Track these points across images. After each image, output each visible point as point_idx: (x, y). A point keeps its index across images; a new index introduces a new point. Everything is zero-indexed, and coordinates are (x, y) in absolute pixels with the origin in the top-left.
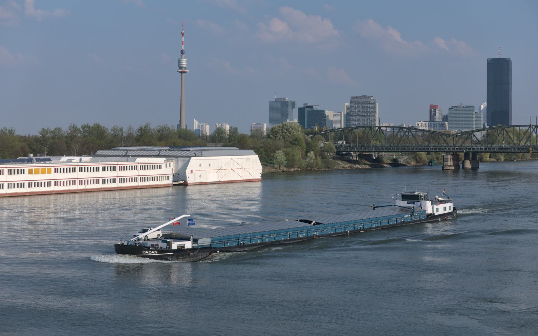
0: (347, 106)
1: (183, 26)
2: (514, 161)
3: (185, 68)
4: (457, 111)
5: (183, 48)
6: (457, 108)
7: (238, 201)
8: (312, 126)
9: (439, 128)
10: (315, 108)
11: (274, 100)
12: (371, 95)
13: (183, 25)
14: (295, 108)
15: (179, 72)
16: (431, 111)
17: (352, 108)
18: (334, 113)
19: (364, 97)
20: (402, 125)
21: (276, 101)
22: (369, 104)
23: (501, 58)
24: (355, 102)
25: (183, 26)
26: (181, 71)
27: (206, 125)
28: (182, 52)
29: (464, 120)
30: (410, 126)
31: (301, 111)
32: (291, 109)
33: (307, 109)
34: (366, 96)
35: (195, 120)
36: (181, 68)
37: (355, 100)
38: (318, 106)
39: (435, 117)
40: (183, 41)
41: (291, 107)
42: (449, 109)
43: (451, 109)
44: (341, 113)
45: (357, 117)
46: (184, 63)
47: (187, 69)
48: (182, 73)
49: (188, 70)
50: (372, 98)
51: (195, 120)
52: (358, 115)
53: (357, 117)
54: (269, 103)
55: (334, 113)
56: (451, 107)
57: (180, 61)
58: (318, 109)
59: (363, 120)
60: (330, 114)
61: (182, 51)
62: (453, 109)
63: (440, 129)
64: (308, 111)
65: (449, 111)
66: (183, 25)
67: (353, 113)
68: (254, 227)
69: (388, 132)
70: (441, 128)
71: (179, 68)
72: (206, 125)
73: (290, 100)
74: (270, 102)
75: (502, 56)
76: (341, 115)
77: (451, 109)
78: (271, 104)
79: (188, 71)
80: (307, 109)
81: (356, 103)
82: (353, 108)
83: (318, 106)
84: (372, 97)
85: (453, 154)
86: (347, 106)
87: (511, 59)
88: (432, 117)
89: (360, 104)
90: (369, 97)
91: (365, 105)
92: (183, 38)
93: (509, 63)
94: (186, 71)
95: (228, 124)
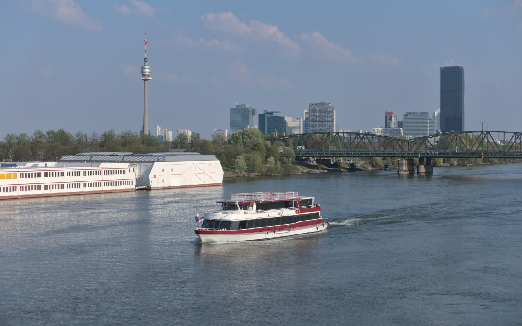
0: (306, 112)
2: (466, 166)
5: (146, 56)
6: (412, 115)
10: (275, 114)
11: (235, 107)
13: (146, 34)
14: (255, 114)
15: (142, 79)
16: (386, 117)
18: (293, 119)
19: (322, 104)
20: (359, 130)
21: (237, 108)
26: (144, 78)
27: (169, 131)
28: (145, 60)
31: (262, 117)
32: (251, 116)
36: (144, 75)
37: (314, 106)
39: (391, 123)
40: (146, 49)
41: (251, 113)
42: (404, 115)
43: (406, 115)
44: (300, 119)
46: (147, 71)
48: (144, 80)
49: (151, 77)
50: (330, 105)
51: (158, 127)
52: (316, 121)
55: (293, 119)
56: (11, 134)
57: (143, 68)
58: (278, 116)
60: (289, 121)
61: (145, 59)
62: (408, 115)
64: (268, 117)
65: (404, 117)
66: (146, 34)
74: (231, 108)
76: (300, 121)
77: (406, 115)
78: (232, 110)
79: (151, 78)
82: (312, 115)
83: (278, 112)
84: (330, 103)
85: (408, 159)
86: (306, 112)
87: (464, 67)
90: (327, 104)
91: (323, 112)
92: (146, 46)
93: (462, 71)
94: (149, 78)
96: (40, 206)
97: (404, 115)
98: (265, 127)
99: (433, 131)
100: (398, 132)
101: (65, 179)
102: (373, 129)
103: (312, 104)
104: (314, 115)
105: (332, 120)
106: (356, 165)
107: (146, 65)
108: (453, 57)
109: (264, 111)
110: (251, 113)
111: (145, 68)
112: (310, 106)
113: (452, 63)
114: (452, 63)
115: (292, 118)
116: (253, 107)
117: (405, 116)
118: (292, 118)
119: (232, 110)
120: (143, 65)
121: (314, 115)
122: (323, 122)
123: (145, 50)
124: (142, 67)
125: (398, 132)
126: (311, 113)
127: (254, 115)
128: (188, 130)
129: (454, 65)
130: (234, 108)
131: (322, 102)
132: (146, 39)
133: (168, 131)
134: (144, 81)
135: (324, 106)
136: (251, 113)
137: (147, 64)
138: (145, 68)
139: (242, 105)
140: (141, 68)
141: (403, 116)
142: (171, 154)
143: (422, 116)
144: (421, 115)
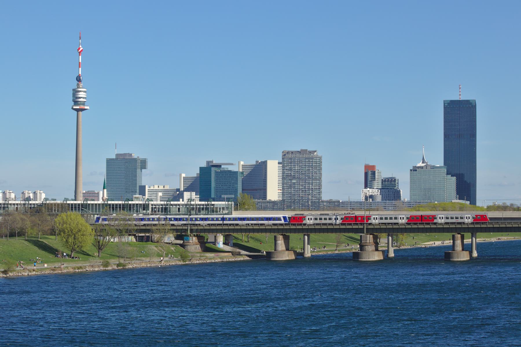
1: (80, 39)
3: (84, 103)
4: (427, 174)
6: (422, 170)
8: (223, 194)
9: (392, 199)
12: (314, 150)
13: (80, 37)
14: (145, 168)
16: (366, 174)
17: (286, 168)
21: (116, 159)
22: (313, 162)
23: (462, 100)
24: (291, 159)
25: (80, 39)
26: (78, 107)
27: (11, 193)
28: (79, 79)
29: (432, 186)
30: (40, 199)
33: (213, 169)
34: (307, 150)
36: (76, 103)
37: (290, 156)
38: (232, 164)
39: (373, 182)
40: (80, 61)
42: (411, 170)
43: (414, 170)
45: (294, 181)
48: (77, 110)
52: (294, 178)
53: (294, 181)
54: (107, 161)
56: (412, 168)
57: (75, 92)
58: (229, 169)
62: (416, 170)
63: (394, 199)
64: (216, 172)
65: (411, 173)
66: (80, 37)
67: (286, 175)
68: (454, 345)
69: (340, 204)
70: (395, 198)
72: (11, 193)
73: (138, 157)
74: (107, 159)
75: (464, 97)
78: (109, 162)
80: (213, 169)
81: (291, 161)
82: (288, 168)
83: (232, 164)
84: (315, 151)
88: (368, 183)
89: (298, 162)
90: (310, 152)
91: (306, 164)
94: (86, 108)
96: (58, 325)
97: (411, 170)
98: (211, 188)
99: (412, 194)
100: (398, 195)
102: (363, 191)
103: (287, 152)
104: (291, 170)
105: (319, 177)
107: (81, 87)
108: (461, 86)
109: (208, 162)
112: (285, 155)
113: (460, 95)
114: (460, 95)
116: (142, 157)
117: (412, 172)
120: (76, 87)
121: (291, 170)
122: (306, 179)
123: (79, 62)
124: (74, 90)
125: (398, 195)
126: (286, 166)
127: (143, 170)
128: (41, 192)
129: (463, 98)
130: (113, 159)
132: (80, 46)
133: (9, 193)
137: (81, 85)
138: (79, 91)
139: (125, 154)
140: (71, 92)
141: (409, 171)
142: (348, 232)
143: (438, 171)
144: (437, 170)
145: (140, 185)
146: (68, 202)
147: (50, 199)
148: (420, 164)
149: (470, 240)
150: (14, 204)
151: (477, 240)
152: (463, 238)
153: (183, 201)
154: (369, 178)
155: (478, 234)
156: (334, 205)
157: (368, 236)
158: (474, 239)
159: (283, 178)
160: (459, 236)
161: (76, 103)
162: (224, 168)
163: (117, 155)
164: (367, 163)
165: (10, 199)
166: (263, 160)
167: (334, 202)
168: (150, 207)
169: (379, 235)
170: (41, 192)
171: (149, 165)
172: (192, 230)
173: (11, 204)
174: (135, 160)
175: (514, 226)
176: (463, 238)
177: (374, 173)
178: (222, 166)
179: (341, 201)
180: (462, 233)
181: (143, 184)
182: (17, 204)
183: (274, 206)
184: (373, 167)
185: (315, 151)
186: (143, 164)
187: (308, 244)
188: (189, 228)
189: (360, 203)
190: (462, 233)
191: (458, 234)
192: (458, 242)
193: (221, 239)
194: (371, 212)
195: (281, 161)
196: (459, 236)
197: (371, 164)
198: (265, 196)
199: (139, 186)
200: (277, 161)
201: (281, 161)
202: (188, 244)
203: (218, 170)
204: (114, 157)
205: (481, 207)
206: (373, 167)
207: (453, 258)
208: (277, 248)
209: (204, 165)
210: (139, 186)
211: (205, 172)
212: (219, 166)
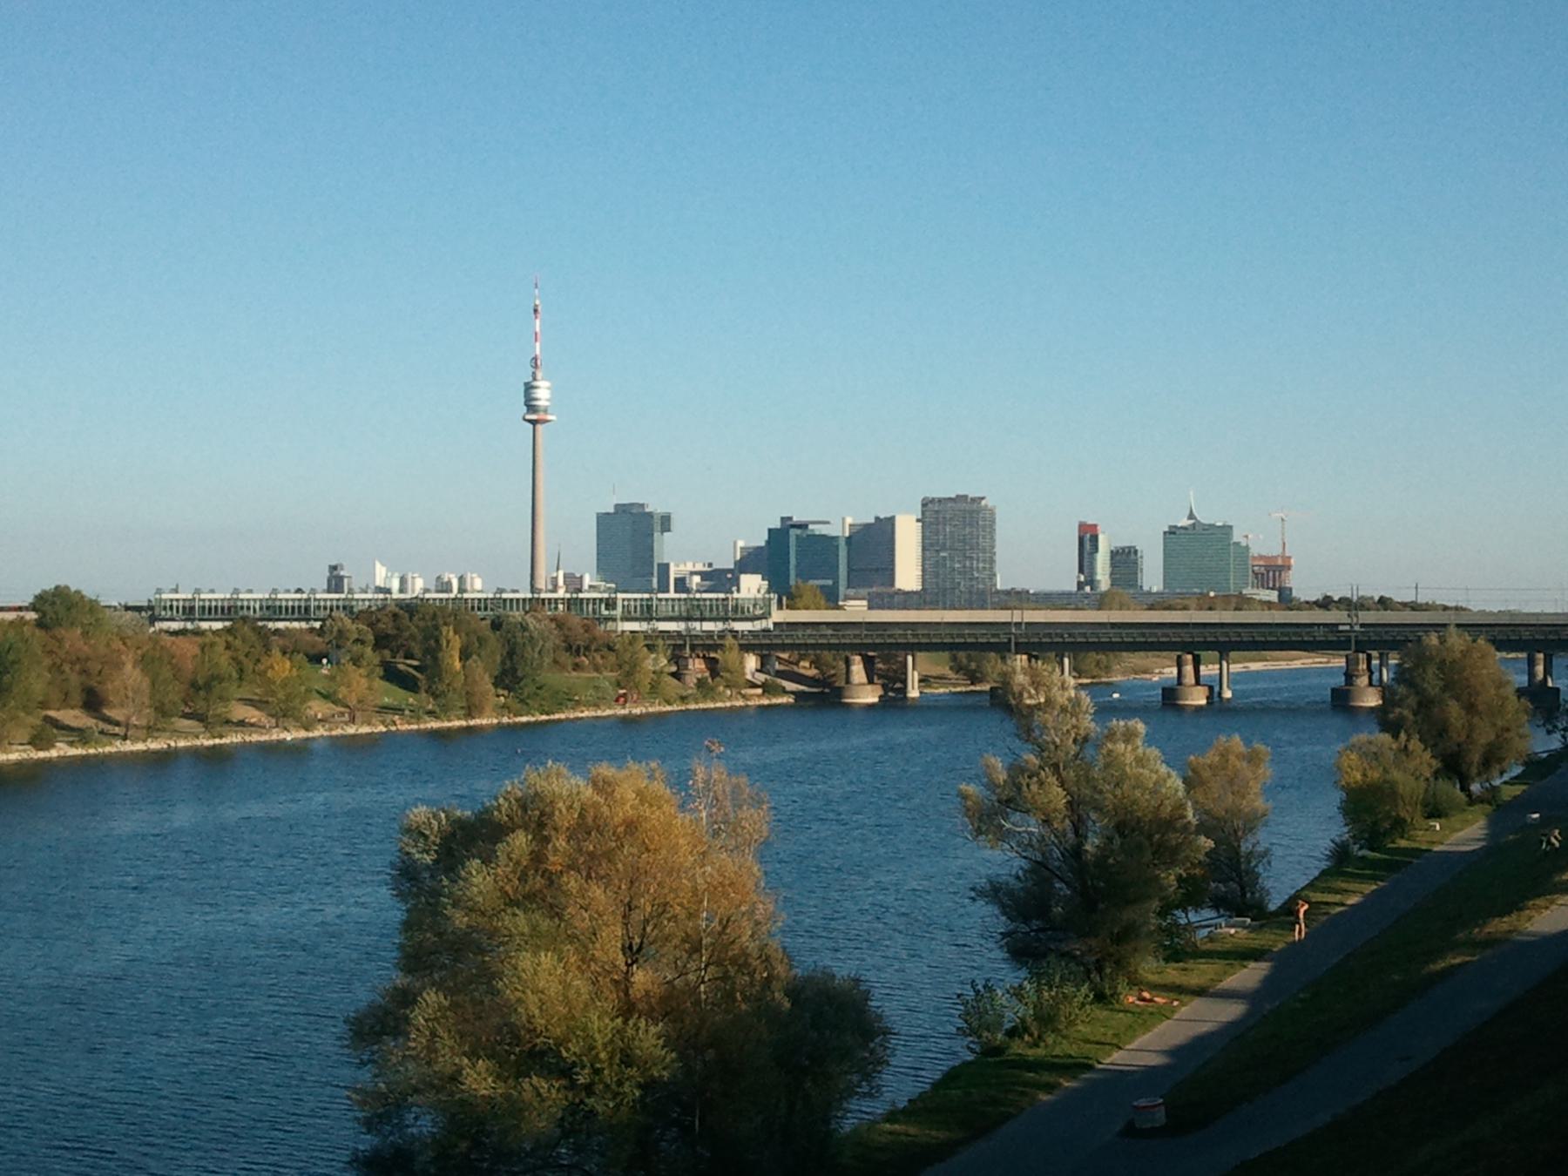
0: (741, 548)
3: (546, 411)
7: (843, 636)
12: (981, 495)
13: (536, 285)
14: (669, 530)
21: (615, 513)
25: (536, 287)
33: (793, 532)
35: (378, 565)
36: (531, 408)
41: (659, 528)
42: (1165, 533)
43: (1171, 533)
45: (942, 554)
46: (543, 394)
47: (549, 411)
49: (552, 414)
51: (378, 565)
52: (944, 548)
53: (942, 554)
56: (1167, 529)
57: (529, 388)
58: (823, 533)
59: (959, 562)
62: (1174, 533)
71: (525, 408)
78: (602, 519)
80: (793, 532)
84: (983, 498)
86: (741, 548)
90: (973, 500)
95: (479, 576)
97: (1165, 533)
101: (1310, 661)
106: (525, 961)
109: (783, 519)
110: (657, 527)
111: (536, 387)
115: (760, 576)
118: (760, 576)
119: (602, 519)
120: (531, 379)
127: (665, 534)
131: (961, 493)
134: (531, 426)
135: (968, 507)
136: (657, 527)
138: (536, 387)
140: (522, 389)
145: (660, 562)
146: (504, 596)
147: (508, 589)
148: (1185, 522)
149: (1217, 666)
150: (363, 600)
151: (1231, 666)
152: (1197, 663)
153: (738, 591)
154: (1088, 546)
155: (1232, 654)
156: (1018, 598)
157: (1018, 657)
158: (1225, 664)
159: (924, 549)
160: (1189, 657)
161: (531, 408)
162: (812, 530)
163: (617, 506)
164: (1083, 520)
165: (540, 591)
166: (889, 515)
167: (1018, 593)
168: (619, 604)
169: (1203, 654)
170: (415, 575)
171: (675, 524)
172: (693, 648)
173: (357, 600)
174: (650, 515)
175: (820, 641)
176: (1197, 663)
177: (1095, 539)
178: (811, 527)
179: (1031, 592)
180: (1196, 653)
181: (665, 561)
182: (370, 600)
183: (908, 600)
184: (1095, 526)
185: (983, 498)
186: (666, 523)
187: (914, 669)
188: (688, 643)
189: (1070, 594)
190: (1196, 653)
191: (1189, 653)
192: (1189, 669)
193: (751, 662)
194: (1025, 612)
195: (920, 517)
196: (1189, 657)
197: (1090, 522)
198: (891, 580)
199: (659, 565)
200: (914, 518)
201: (920, 517)
202: (685, 672)
203: (798, 532)
204: (612, 510)
205: (91, 601)
206: (1095, 526)
207: (1179, 699)
208: (852, 679)
209: (777, 525)
210: (659, 565)
211: (778, 537)
212: (803, 526)
